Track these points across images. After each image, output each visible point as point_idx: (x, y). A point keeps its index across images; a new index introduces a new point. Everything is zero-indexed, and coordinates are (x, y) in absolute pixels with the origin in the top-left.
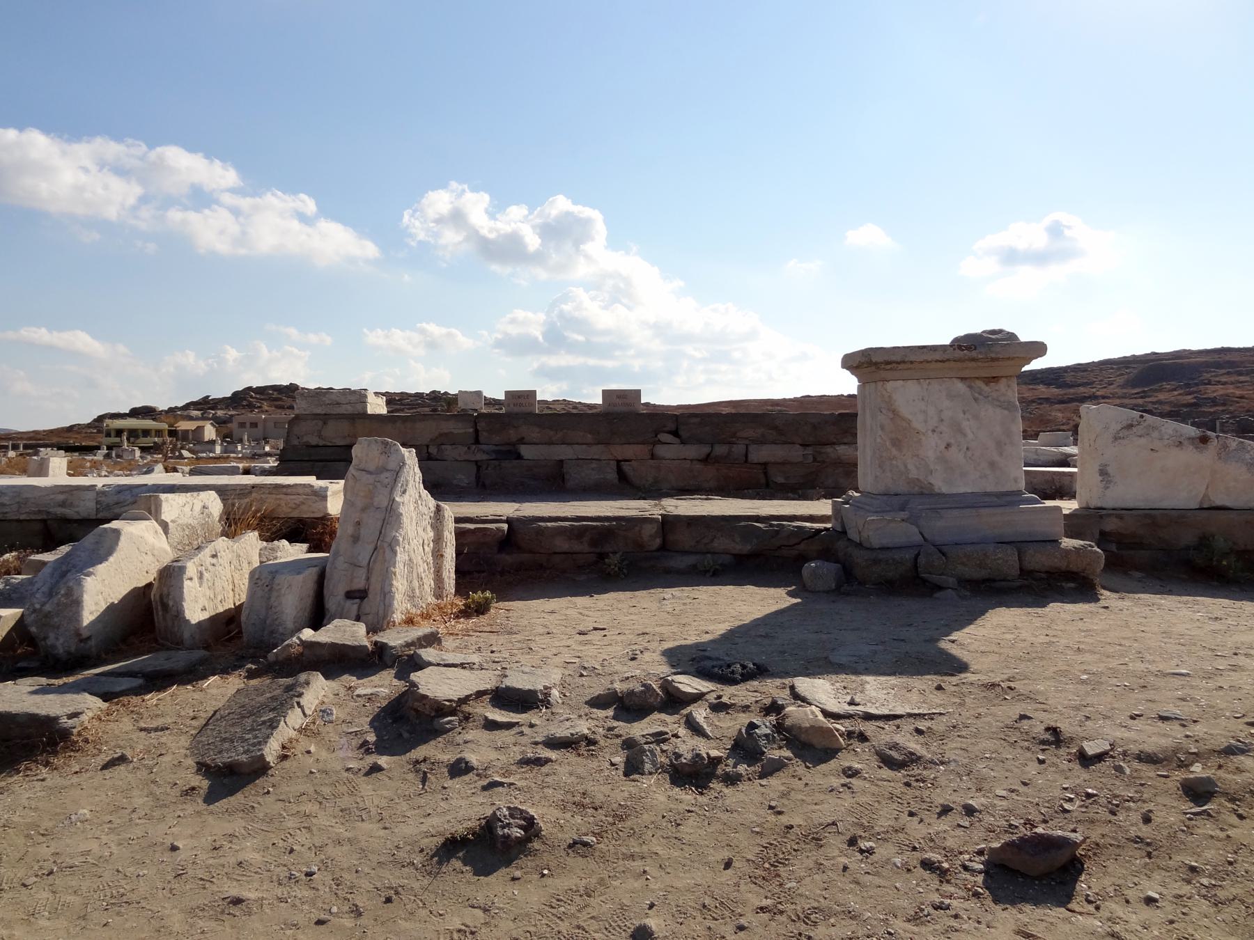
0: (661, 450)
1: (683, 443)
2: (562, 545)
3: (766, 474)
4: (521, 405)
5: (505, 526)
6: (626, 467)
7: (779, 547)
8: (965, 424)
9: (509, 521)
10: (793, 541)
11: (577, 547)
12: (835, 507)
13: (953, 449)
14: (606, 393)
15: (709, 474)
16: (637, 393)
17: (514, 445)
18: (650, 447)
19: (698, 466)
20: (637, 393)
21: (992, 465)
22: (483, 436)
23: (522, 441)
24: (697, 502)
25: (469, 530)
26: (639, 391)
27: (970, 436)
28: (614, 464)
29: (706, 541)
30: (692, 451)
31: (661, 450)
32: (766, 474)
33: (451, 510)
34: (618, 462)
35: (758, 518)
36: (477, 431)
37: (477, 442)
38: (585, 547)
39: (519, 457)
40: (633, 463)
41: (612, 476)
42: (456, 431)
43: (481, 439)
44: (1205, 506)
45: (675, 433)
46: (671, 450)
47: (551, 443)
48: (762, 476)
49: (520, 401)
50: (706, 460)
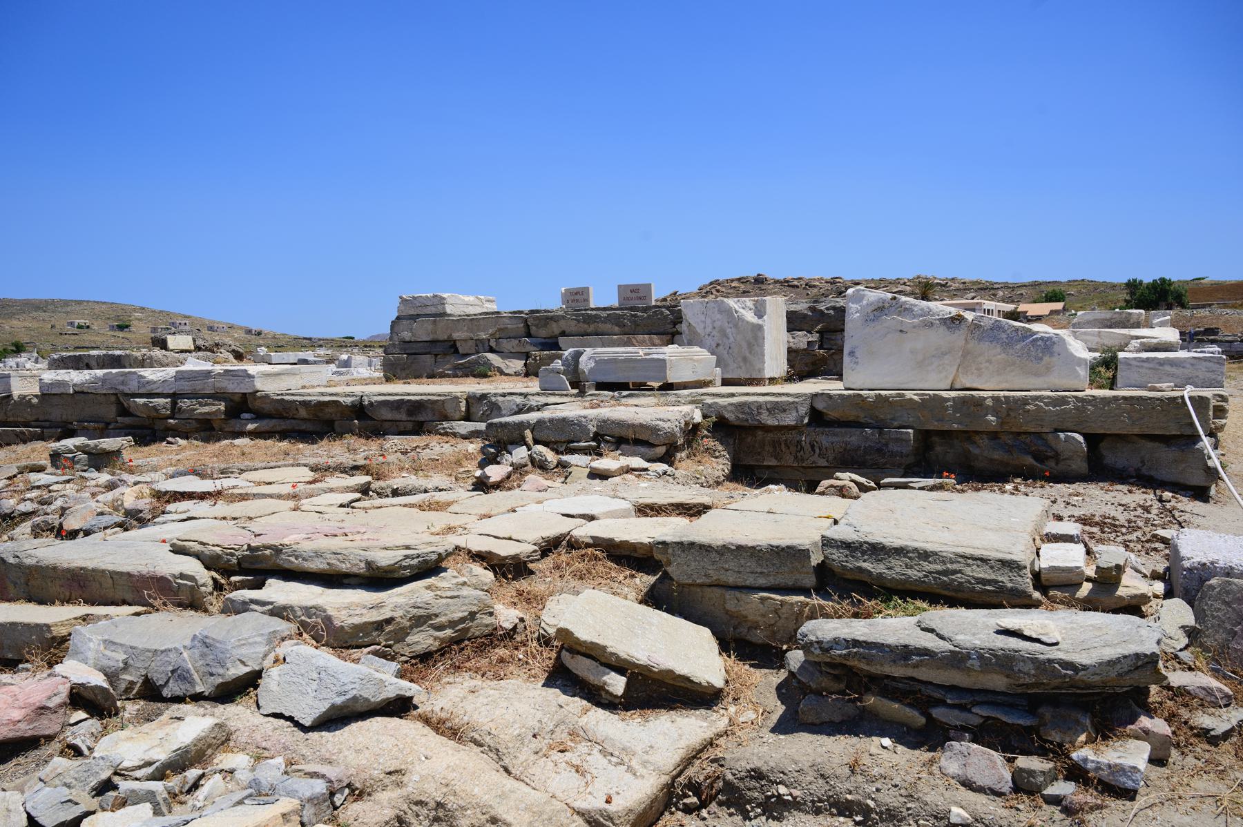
2: (386, 414)
4: (577, 301)
8: (728, 330)
11: (397, 416)
13: (721, 347)
17: (556, 337)
21: (745, 359)
22: (533, 330)
23: (563, 334)
27: (732, 339)
36: (528, 326)
44: (958, 386)
49: (578, 297)
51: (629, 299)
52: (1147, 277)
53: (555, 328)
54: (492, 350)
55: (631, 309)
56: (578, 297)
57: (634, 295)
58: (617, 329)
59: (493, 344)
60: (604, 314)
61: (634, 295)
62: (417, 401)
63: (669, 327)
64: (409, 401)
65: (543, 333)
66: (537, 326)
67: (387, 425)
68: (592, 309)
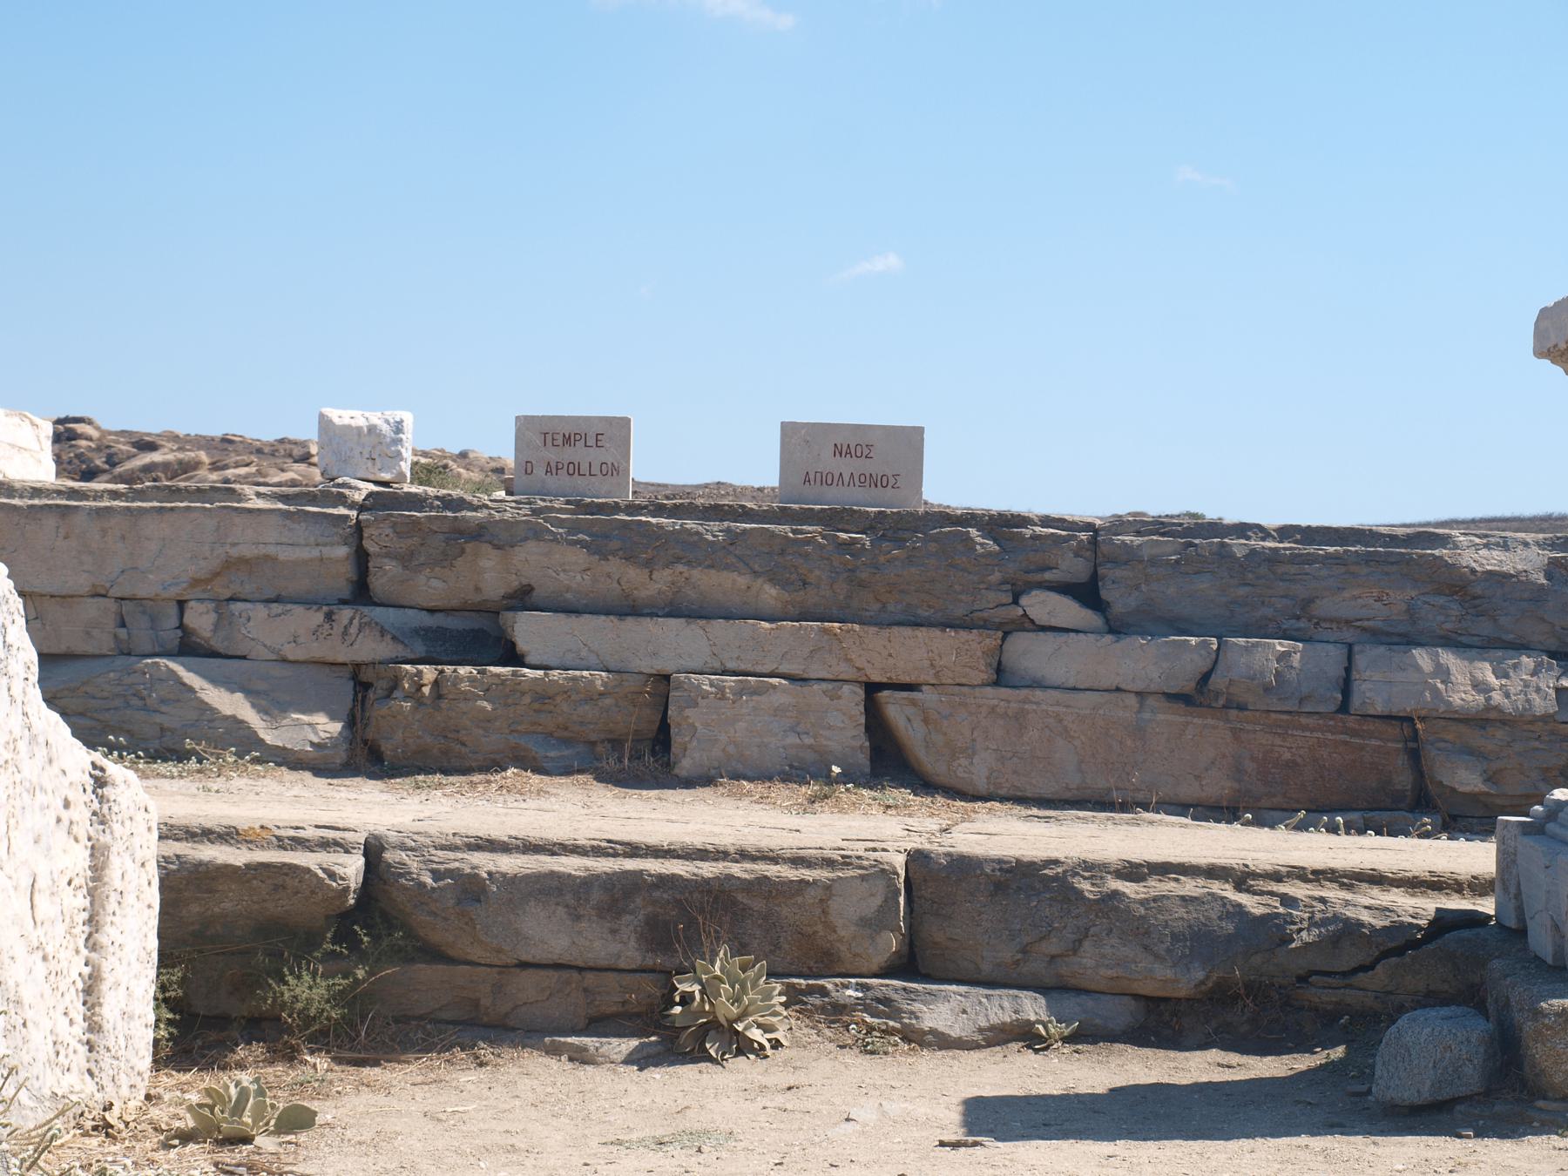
0: (1029, 653)
1: (1116, 628)
2: (548, 935)
3: (1415, 756)
4: (574, 469)
5: (352, 867)
6: (895, 708)
7: (1303, 979)
9: (373, 850)
10: (1346, 961)
12: (1506, 860)
14: (793, 435)
15: (1204, 744)
16: (615, 433)
17: (491, 611)
18: (992, 640)
19: (1165, 718)
20: (615, 433)
22: (385, 574)
23: (523, 599)
24: (1091, 828)
25: (228, 871)
26: (920, 431)
28: (852, 698)
29: (1052, 947)
30: (1144, 661)
31: (1029, 653)
32: (1415, 756)
33: (147, 801)
34: (872, 689)
35: (1242, 878)
36: (362, 558)
37: (361, 593)
38: (630, 952)
39: (513, 657)
40: (927, 696)
41: (843, 727)
42: (285, 554)
43: (378, 583)
45: (1087, 593)
46: (1067, 653)
47: (629, 609)
48: (1401, 761)
50: (1196, 696)
51: (826, 480)
52: (63, 416)
53: (490, 575)
54: (189, 648)
55: (834, 519)
56: (568, 454)
57: (846, 466)
58: (770, 594)
59: (201, 619)
60: (714, 530)
61: (846, 466)
62: (703, 885)
63: (991, 601)
64: (665, 881)
65: (432, 587)
66: (406, 559)
67: (528, 986)
68: (632, 509)
